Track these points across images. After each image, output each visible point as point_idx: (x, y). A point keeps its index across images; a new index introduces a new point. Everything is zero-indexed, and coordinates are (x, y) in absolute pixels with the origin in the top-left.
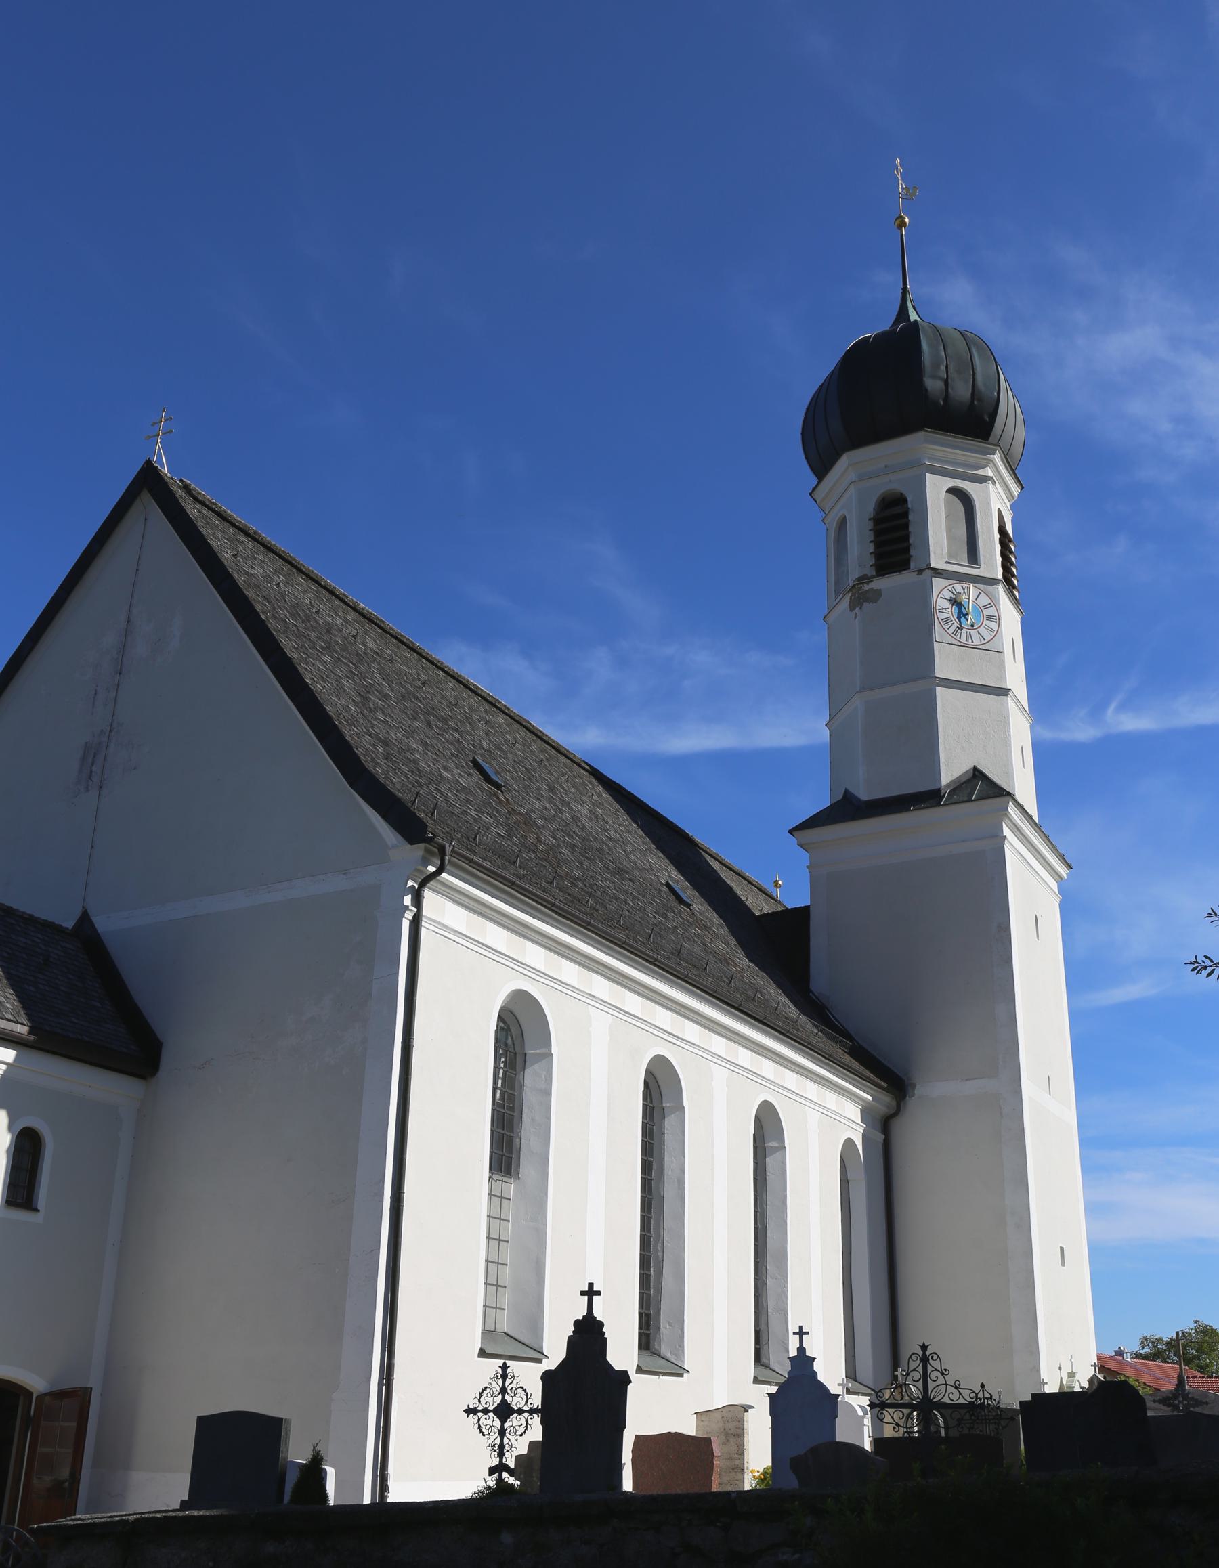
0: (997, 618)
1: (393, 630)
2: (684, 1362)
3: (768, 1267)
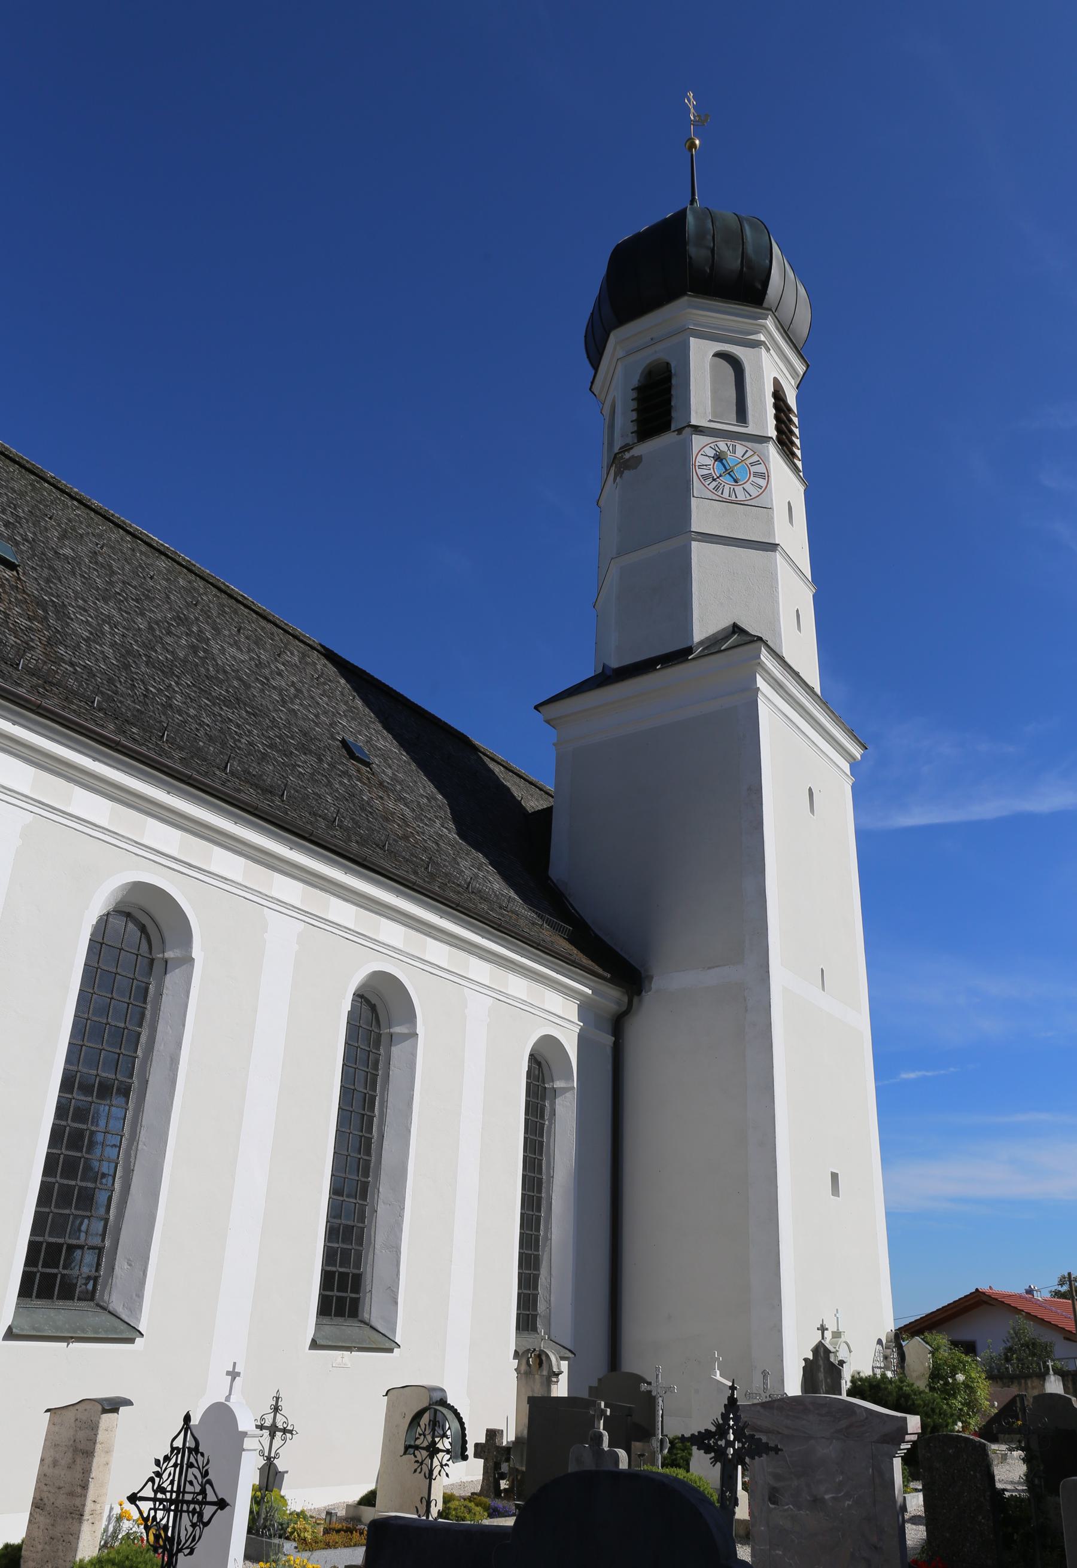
0: (766, 475)
1: (11, 452)
2: (139, 1320)
3: (381, 1189)
